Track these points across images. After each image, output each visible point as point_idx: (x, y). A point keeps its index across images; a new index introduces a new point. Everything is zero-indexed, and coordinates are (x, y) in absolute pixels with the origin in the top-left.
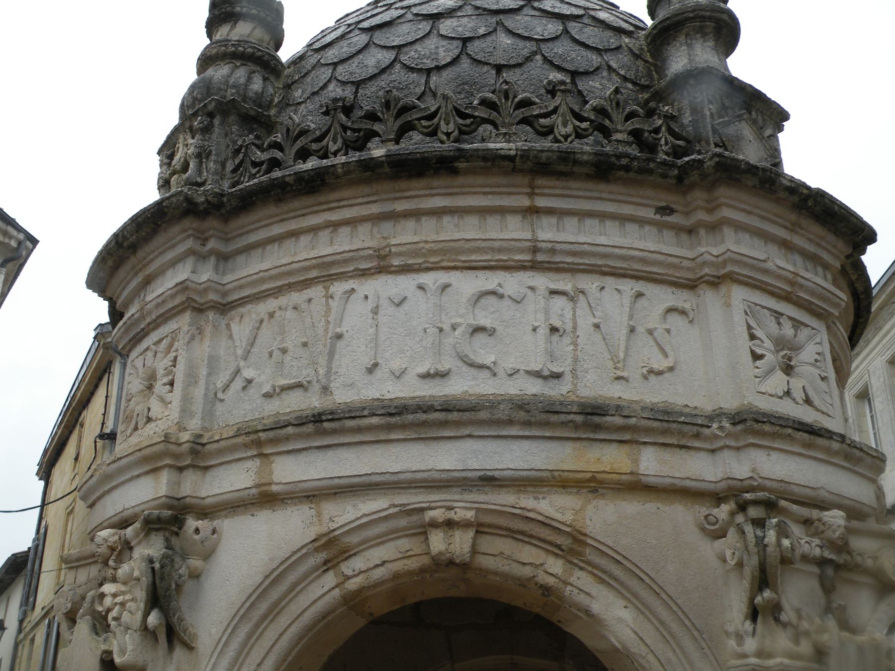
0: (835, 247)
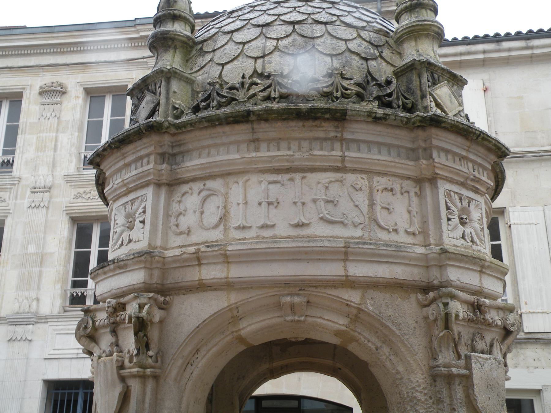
0: (145, 144)
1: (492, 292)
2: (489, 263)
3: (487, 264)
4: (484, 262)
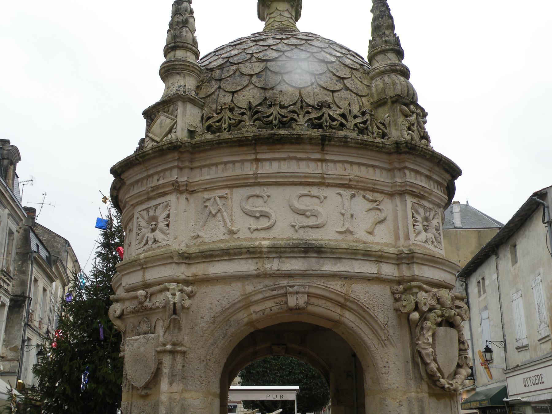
1: (155, 280)
2: (144, 260)
3: (142, 261)
4: (139, 261)
